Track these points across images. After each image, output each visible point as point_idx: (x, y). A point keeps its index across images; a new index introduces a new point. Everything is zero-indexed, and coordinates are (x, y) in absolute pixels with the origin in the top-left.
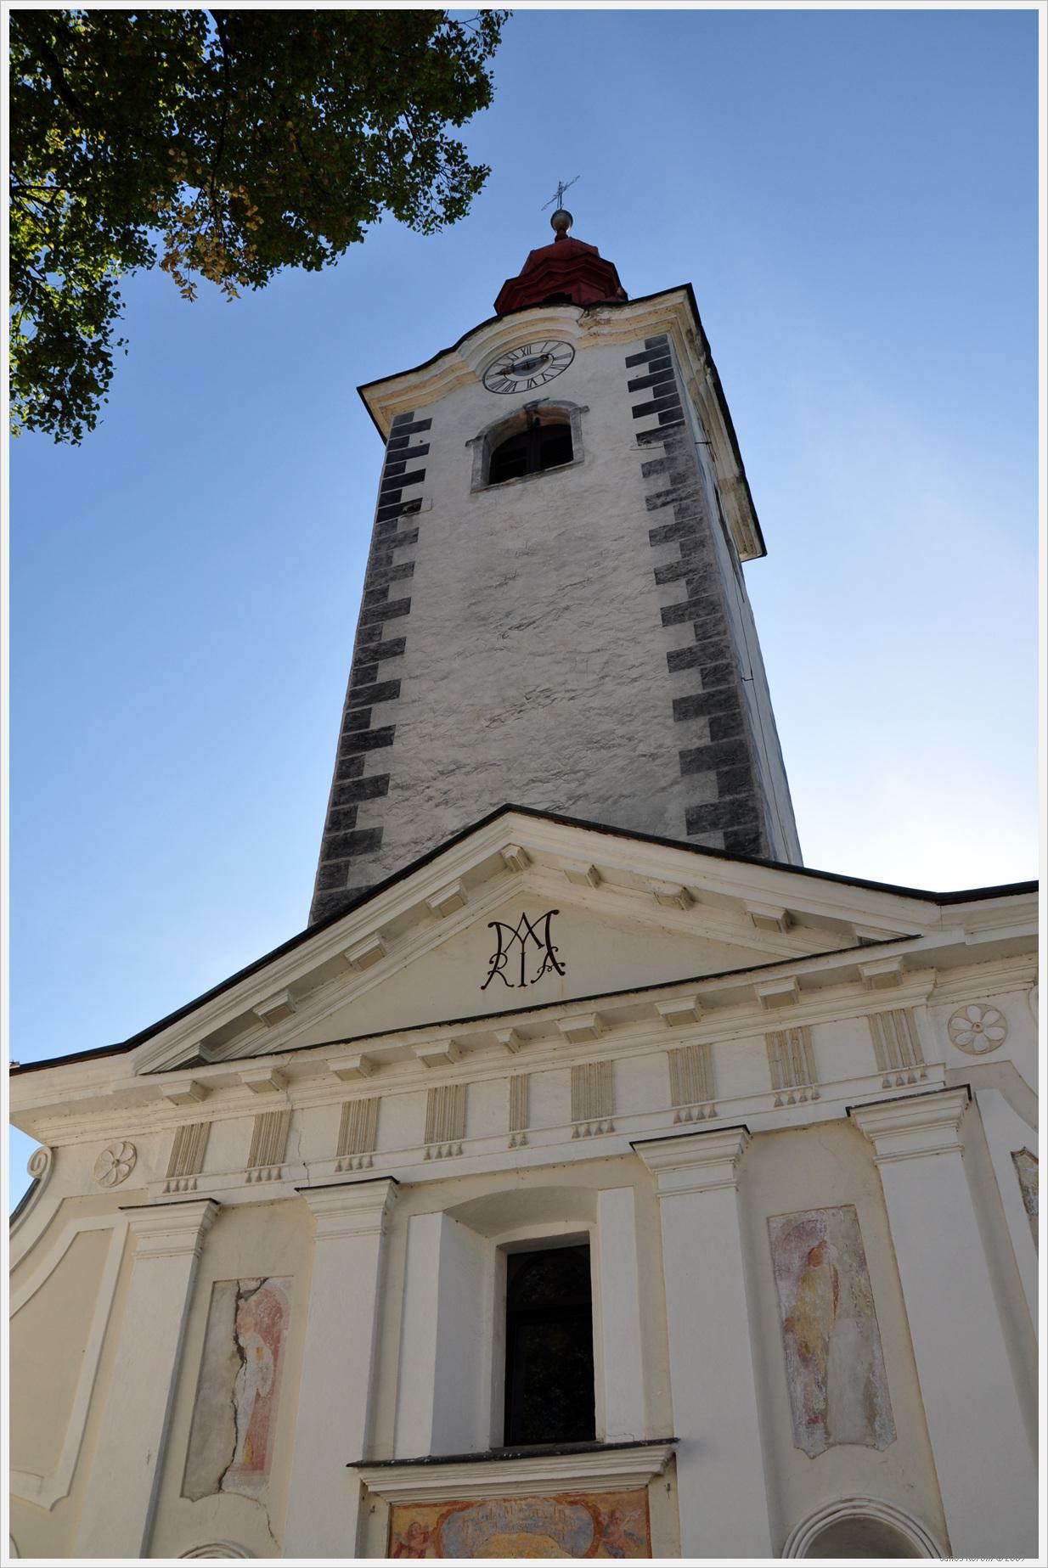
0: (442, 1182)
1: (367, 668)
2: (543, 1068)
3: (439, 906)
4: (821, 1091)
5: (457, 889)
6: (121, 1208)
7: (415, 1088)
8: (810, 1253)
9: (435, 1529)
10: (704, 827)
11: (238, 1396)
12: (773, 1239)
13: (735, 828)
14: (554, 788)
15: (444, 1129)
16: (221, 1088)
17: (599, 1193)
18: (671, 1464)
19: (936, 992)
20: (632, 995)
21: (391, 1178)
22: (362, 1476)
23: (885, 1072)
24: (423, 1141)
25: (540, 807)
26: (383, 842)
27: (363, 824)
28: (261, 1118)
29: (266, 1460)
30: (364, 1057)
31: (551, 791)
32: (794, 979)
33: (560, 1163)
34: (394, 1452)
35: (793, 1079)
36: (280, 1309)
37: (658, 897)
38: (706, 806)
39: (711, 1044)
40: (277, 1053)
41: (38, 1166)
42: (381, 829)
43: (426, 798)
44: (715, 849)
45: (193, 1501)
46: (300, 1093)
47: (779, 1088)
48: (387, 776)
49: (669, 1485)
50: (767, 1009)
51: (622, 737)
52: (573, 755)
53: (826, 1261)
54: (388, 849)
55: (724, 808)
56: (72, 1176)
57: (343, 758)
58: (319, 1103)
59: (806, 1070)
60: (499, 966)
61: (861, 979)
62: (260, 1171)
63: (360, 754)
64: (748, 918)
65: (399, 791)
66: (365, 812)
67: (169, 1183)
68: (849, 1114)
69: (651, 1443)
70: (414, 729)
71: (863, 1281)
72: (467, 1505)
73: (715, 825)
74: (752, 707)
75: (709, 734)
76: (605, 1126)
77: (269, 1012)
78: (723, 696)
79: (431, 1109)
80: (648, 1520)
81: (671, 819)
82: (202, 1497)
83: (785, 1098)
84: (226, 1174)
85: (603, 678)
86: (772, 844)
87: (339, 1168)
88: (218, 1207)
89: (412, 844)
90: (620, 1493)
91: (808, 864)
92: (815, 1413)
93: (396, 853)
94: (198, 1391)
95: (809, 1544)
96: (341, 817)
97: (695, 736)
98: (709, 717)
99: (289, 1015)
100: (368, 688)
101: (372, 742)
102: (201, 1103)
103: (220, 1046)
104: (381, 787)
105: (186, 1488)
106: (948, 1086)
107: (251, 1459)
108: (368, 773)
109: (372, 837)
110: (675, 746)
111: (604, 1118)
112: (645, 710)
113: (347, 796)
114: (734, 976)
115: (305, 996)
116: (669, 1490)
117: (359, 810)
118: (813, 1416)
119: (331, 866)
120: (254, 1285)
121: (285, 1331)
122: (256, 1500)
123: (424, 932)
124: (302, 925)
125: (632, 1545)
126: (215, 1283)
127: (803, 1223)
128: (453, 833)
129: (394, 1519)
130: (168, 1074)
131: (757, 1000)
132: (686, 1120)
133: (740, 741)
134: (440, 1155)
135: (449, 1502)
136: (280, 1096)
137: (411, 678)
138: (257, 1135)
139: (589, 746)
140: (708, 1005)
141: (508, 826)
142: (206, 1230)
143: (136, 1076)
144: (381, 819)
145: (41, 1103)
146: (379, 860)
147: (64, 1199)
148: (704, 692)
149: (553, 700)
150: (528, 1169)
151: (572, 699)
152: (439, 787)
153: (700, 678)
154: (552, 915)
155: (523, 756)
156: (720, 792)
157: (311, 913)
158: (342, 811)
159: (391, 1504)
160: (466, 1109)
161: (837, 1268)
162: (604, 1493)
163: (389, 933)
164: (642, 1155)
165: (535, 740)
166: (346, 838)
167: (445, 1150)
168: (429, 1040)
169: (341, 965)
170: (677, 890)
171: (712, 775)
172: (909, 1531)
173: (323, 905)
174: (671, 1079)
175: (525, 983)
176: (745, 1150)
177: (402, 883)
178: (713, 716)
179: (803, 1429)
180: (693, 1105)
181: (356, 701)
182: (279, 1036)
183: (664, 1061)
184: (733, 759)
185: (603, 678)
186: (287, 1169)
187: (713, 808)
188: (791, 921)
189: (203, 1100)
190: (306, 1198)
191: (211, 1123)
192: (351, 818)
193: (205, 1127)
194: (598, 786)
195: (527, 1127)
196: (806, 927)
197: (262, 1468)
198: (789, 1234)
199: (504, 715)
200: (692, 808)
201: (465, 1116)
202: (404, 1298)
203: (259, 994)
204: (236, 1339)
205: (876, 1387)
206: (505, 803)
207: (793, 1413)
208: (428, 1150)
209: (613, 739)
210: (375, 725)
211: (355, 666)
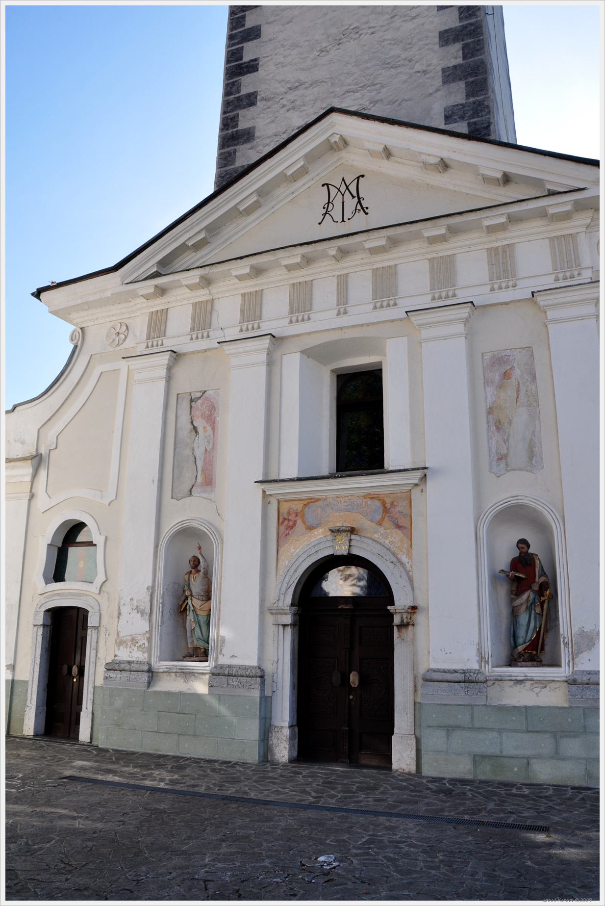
0: (299, 336)
1: (238, 18)
2: (357, 269)
3: (292, 175)
4: (518, 282)
5: (302, 163)
6: (123, 358)
7: (281, 284)
8: (505, 373)
9: (301, 511)
10: (455, 119)
11: (196, 451)
12: (485, 365)
13: (475, 120)
14: (361, 96)
15: (299, 306)
16: (171, 289)
17: (388, 340)
18: (424, 479)
19: (592, 224)
20: (408, 225)
21: (271, 334)
22: (262, 487)
23: (557, 271)
24: (288, 314)
25: (353, 109)
26: (255, 136)
27: (243, 125)
28: (195, 305)
29: (213, 481)
30: (252, 267)
31: (359, 98)
32: (506, 215)
33: (366, 324)
34: (279, 476)
35: (502, 275)
36: (214, 406)
37: (425, 165)
38: (457, 105)
39: (455, 254)
40: (201, 267)
41: (75, 338)
42: (254, 127)
43: (281, 106)
44: (462, 133)
45: (178, 500)
46: (217, 289)
47: (493, 280)
48: (256, 92)
49: (422, 489)
50: (489, 233)
51: (405, 59)
52: (374, 73)
53: (514, 377)
54: (259, 140)
55: (469, 106)
56: (93, 345)
57: (227, 82)
58: (227, 295)
59: (510, 270)
60: (329, 210)
61: (547, 215)
62: (197, 334)
63: (238, 79)
64: (480, 177)
65: (264, 102)
66: (243, 117)
67: (148, 343)
68: (533, 296)
69: (413, 469)
70: (271, 59)
71: (533, 388)
72: (318, 500)
73: (462, 118)
74: (492, 35)
75: (461, 56)
76: (391, 303)
77: (194, 244)
78: (473, 28)
79: (292, 295)
80: (411, 506)
81: (435, 115)
82: (182, 498)
83: (496, 286)
84: (179, 336)
85: (393, 17)
86: (498, 130)
87: (241, 330)
88: (175, 354)
89: (274, 137)
90: (396, 493)
91: (520, 142)
92: (501, 455)
93: (265, 142)
94: (175, 449)
95: (493, 515)
96: (229, 121)
97: (452, 57)
98: (462, 43)
99: (207, 244)
100: (240, 32)
101: (245, 70)
102: (161, 298)
103: (169, 264)
104: (252, 100)
105: (174, 494)
106: (593, 280)
107: (205, 481)
108: (244, 91)
109: (249, 133)
110: (439, 64)
111: (391, 298)
112: (420, 40)
113: (232, 107)
114: (470, 213)
115: (215, 233)
116: (422, 492)
117: (240, 116)
118: (500, 457)
119: (225, 153)
120: (199, 395)
121: (217, 418)
122: (210, 499)
123: (283, 191)
124: (210, 190)
125: (402, 516)
126: (178, 394)
127: (502, 356)
128: (298, 128)
129: (280, 507)
130: (141, 282)
131: (483, 228)
132: (438, 299)
133: (482, 59)
134: (297, 321)
135: (308, 498)
136: (205, 291)
137: (267, 23)
138: (194, 313)
139: (384, 66)
140: (454, 231)
141: (332, 121)
142: (170, 367)
143: (122, 285)
144: (253, 120)
145: (72, 304)
146: (254, 147)
147: (91, 355)
148: (460, 24)
149: (360, 35)
150: (347, 327)
151: (373, 33)
152: (289, 98)
153: (458, 14)
154: (361, 178)
155: (341, 75)
156: (466, 96)
157: (215, 182)
158: (229, 117)
159: (278, 500)
160: (311, 295)
161: (520, 381)
162: (388, 494)
163: (262, 192)
164: (413, 319)
165: (349, 63)
166: (233, 134)
167: (300, 318)
168: (289, 255)
169: (234, 213)
170: (437, 160)
171: (462, 84)
172: (544, 510)
173: (222, 177)
174: (430, 275)
175: (345, 220)
176: (471, 316)
177: (269, 161)
178: (465, 42)
179: (494, 463)
180: (442, 290)
181: (233, 42)
182: (202, 257)
183: (427, 265)
184: (476, 73)
185: (393, 17)
186: (212, 332)
187: (461, 107)
188: (507, 179)
189: (162, 296)
190: (224, 347)
191: (167, 309)
192: (235, 121)
193: (165, 311)
194: (390, 94)
195: (347, 304)
196: (516, 183)
197: (211, 485)
198: (494, 362)
199: (329, 47)
200: (448, 107)
201: (311, 298)
202: (281, 398)
203: (188, 233)
204: (192, 422)
205: (535, 443)
206: (330, 107)
207: (490, 455)
208: (291, 318)
209: (399, 61)
210: (246, 58)
211: (231, 16)
